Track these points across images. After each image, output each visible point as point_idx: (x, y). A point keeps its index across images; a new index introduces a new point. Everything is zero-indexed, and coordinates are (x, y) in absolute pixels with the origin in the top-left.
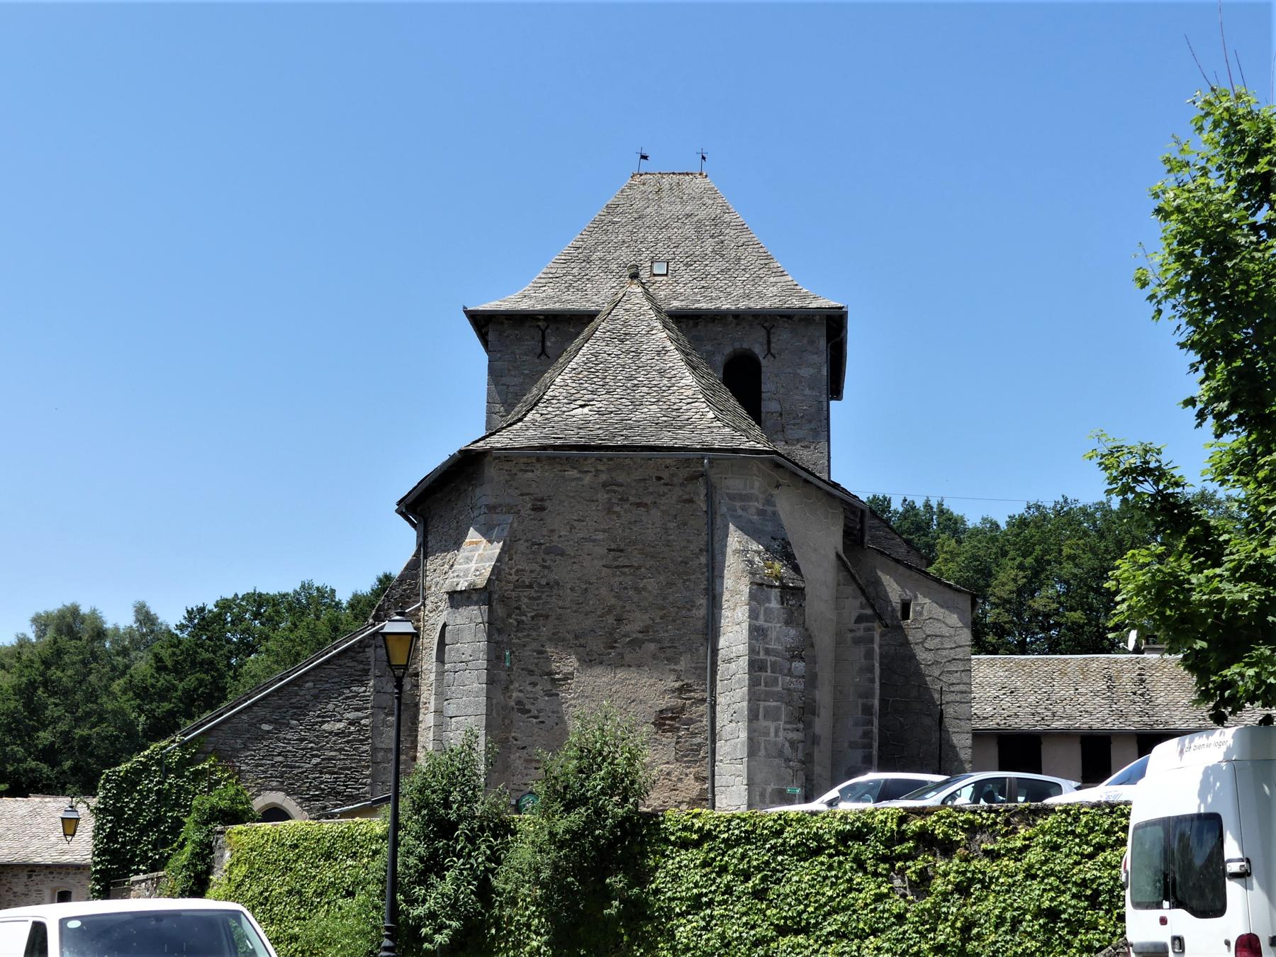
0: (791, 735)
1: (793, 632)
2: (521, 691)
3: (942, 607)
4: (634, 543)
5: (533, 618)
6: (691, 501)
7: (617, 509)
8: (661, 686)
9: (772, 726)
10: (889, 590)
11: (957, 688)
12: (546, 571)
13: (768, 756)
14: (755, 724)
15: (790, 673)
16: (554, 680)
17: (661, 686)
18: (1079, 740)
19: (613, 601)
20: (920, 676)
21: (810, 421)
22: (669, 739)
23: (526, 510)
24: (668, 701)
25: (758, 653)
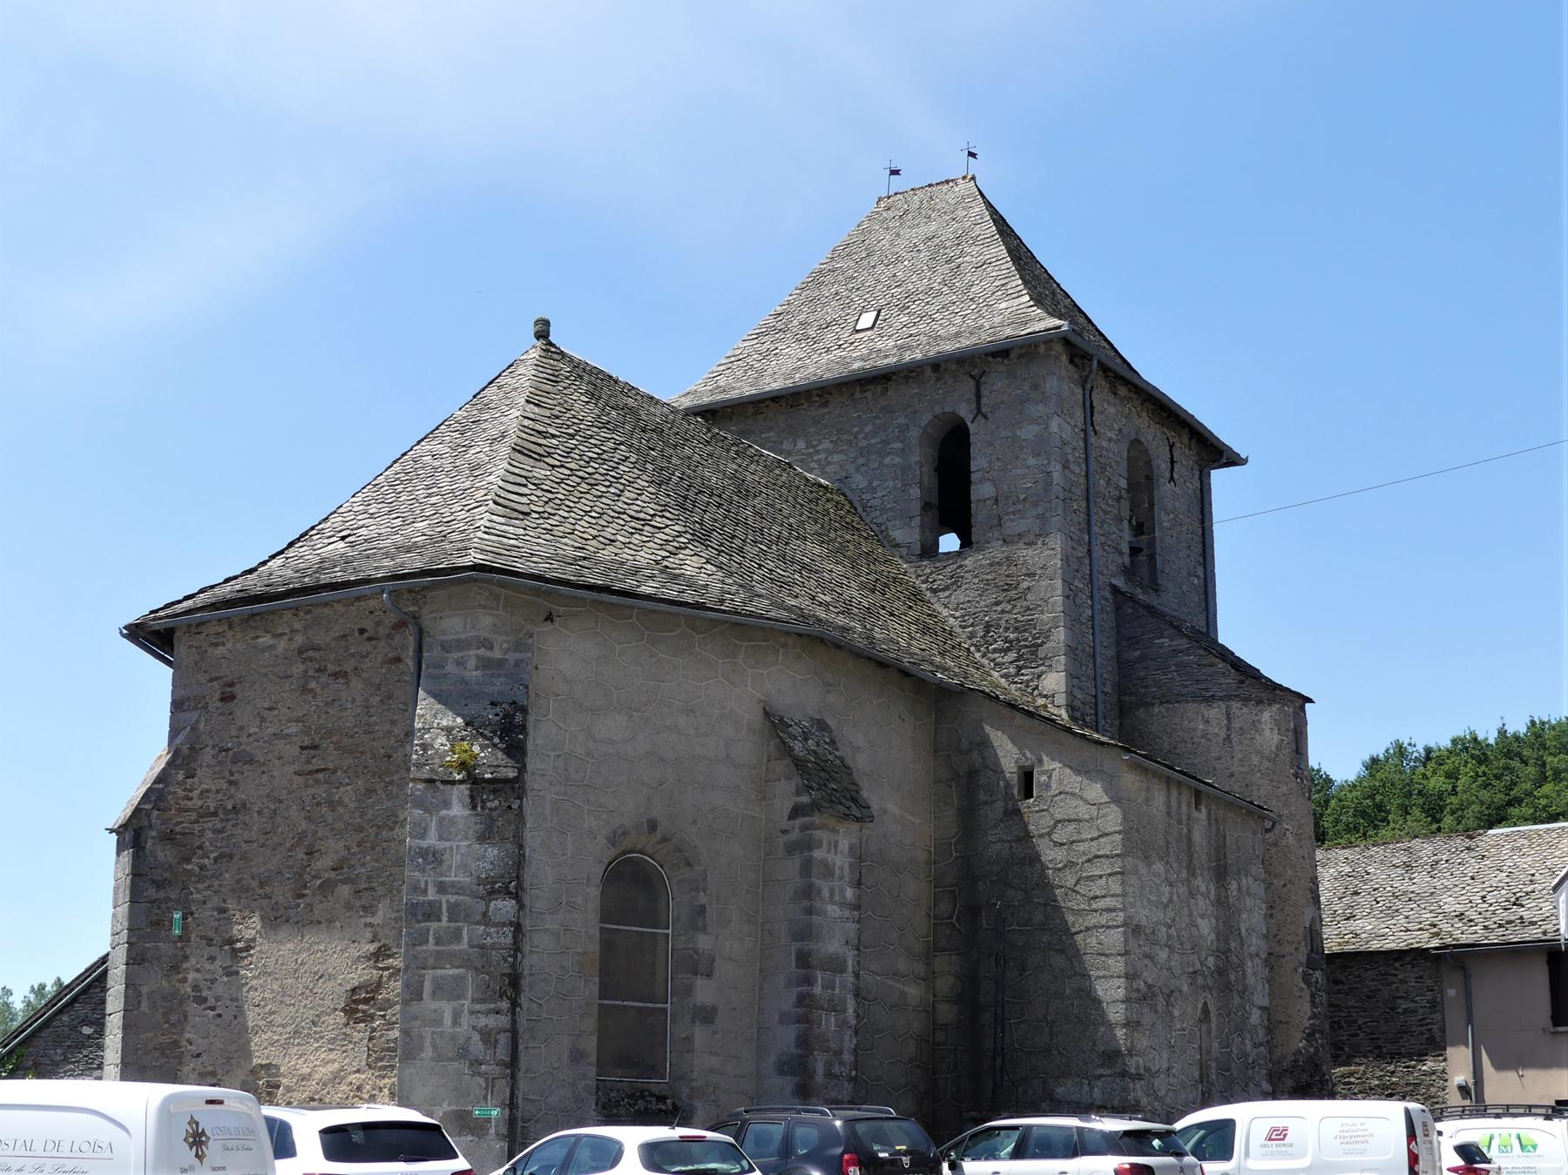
0: (483, 1021)
1: (492, 852)
2: (198, 970)
3: (1078, 772)
4: (330, 733)
5: (216, 860)
6: (398, 660)
7: (312, 685)
8: (353, 952)
9: (447, 1008)
10: (1000, 753)
11: (1101, 904)
12: (233, 789)
13: (439, 1057)
14: (415, 1008)
15: (485, 919)
16: (234, 951)
17: (353, 952)
18: (1544, 958)
19: (304, 825)
20: (1045, 886)
21: (1036, 505)
22: (360, 1032)
23: (215, 704)
24: (362, 974)
25: (425, 891)
